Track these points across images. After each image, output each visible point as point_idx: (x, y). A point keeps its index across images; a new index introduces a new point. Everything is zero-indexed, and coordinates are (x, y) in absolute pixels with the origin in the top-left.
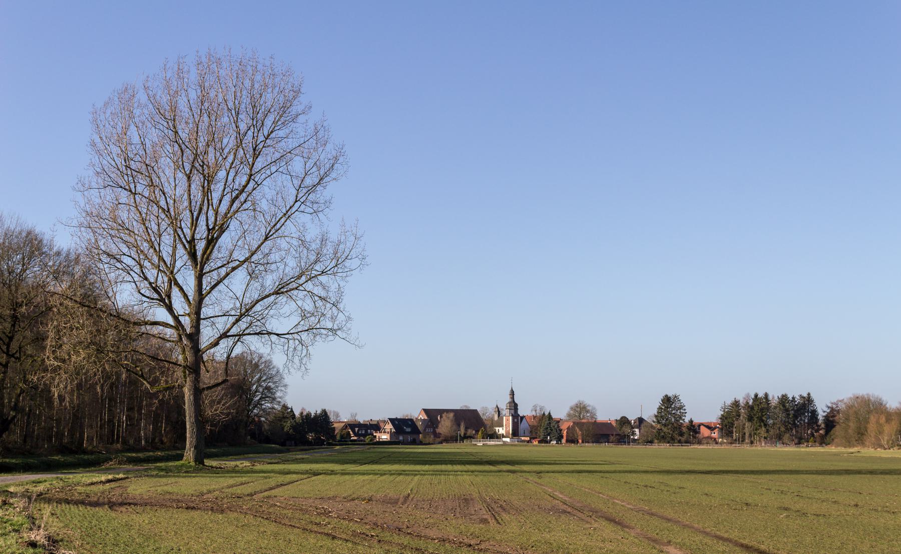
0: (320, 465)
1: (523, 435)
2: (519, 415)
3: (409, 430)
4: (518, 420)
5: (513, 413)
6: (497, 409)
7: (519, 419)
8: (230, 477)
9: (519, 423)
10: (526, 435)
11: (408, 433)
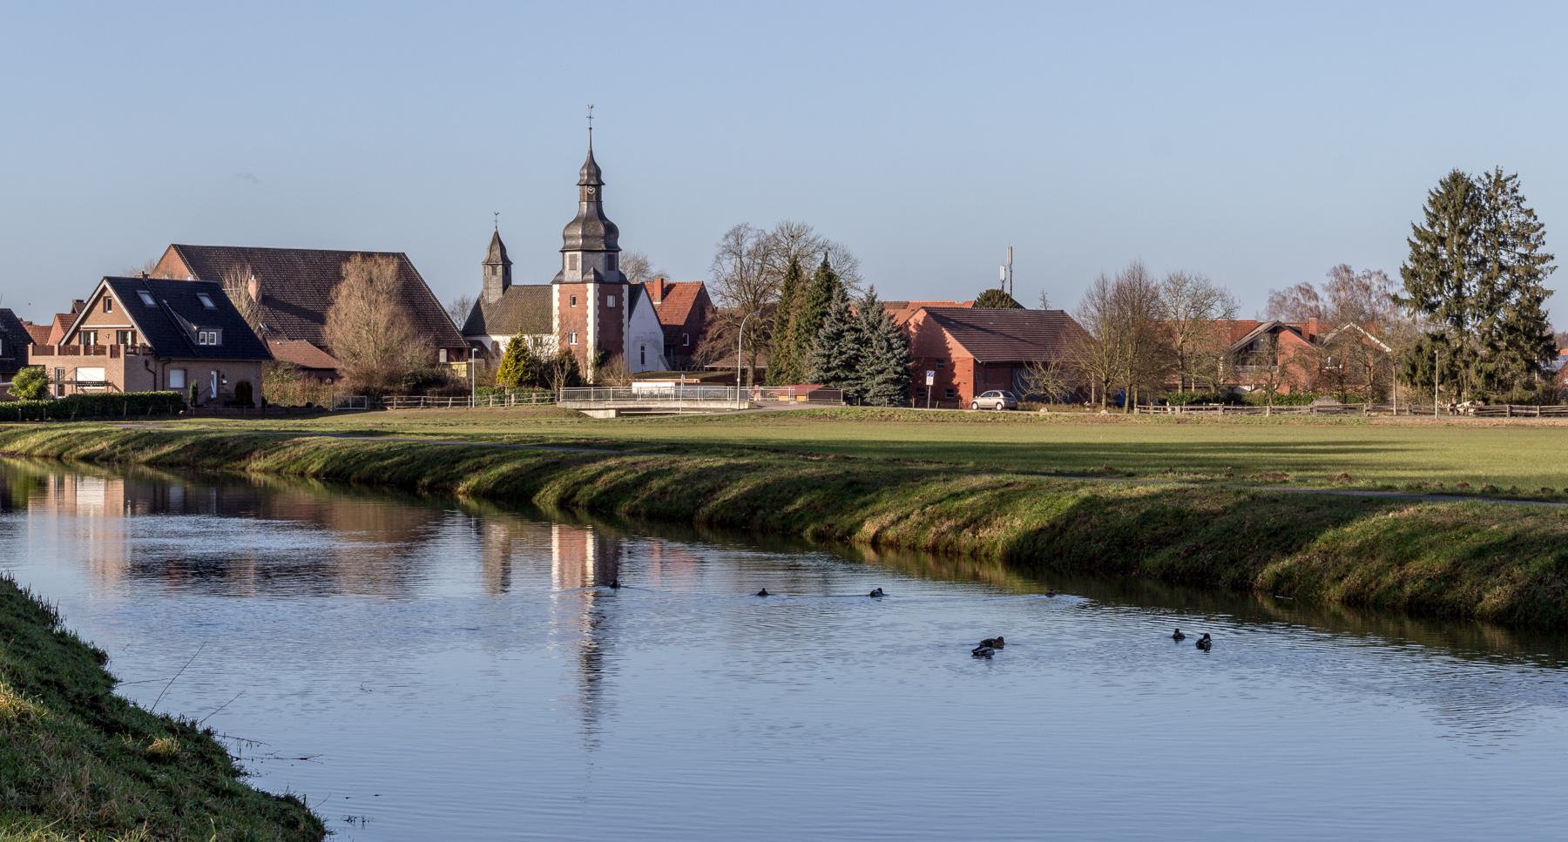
0: (1041, 441)
1: (639, 368)
2: (622, 279)
3: (210, 337)
4: (619, 300)
5: (601, 270)
6: (498, 252)
7: (626, 295)
8: (1452, 468)
9: (625, 312)
10: (648, 367)
11: (209, 353)
